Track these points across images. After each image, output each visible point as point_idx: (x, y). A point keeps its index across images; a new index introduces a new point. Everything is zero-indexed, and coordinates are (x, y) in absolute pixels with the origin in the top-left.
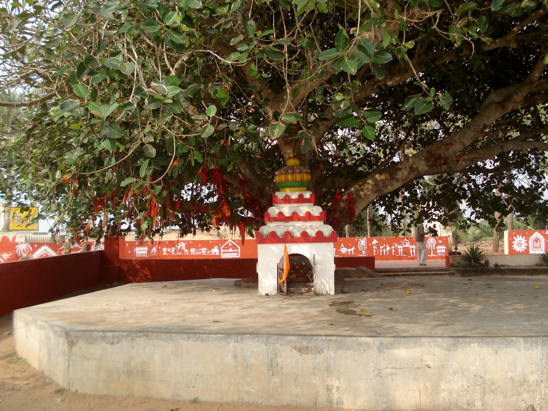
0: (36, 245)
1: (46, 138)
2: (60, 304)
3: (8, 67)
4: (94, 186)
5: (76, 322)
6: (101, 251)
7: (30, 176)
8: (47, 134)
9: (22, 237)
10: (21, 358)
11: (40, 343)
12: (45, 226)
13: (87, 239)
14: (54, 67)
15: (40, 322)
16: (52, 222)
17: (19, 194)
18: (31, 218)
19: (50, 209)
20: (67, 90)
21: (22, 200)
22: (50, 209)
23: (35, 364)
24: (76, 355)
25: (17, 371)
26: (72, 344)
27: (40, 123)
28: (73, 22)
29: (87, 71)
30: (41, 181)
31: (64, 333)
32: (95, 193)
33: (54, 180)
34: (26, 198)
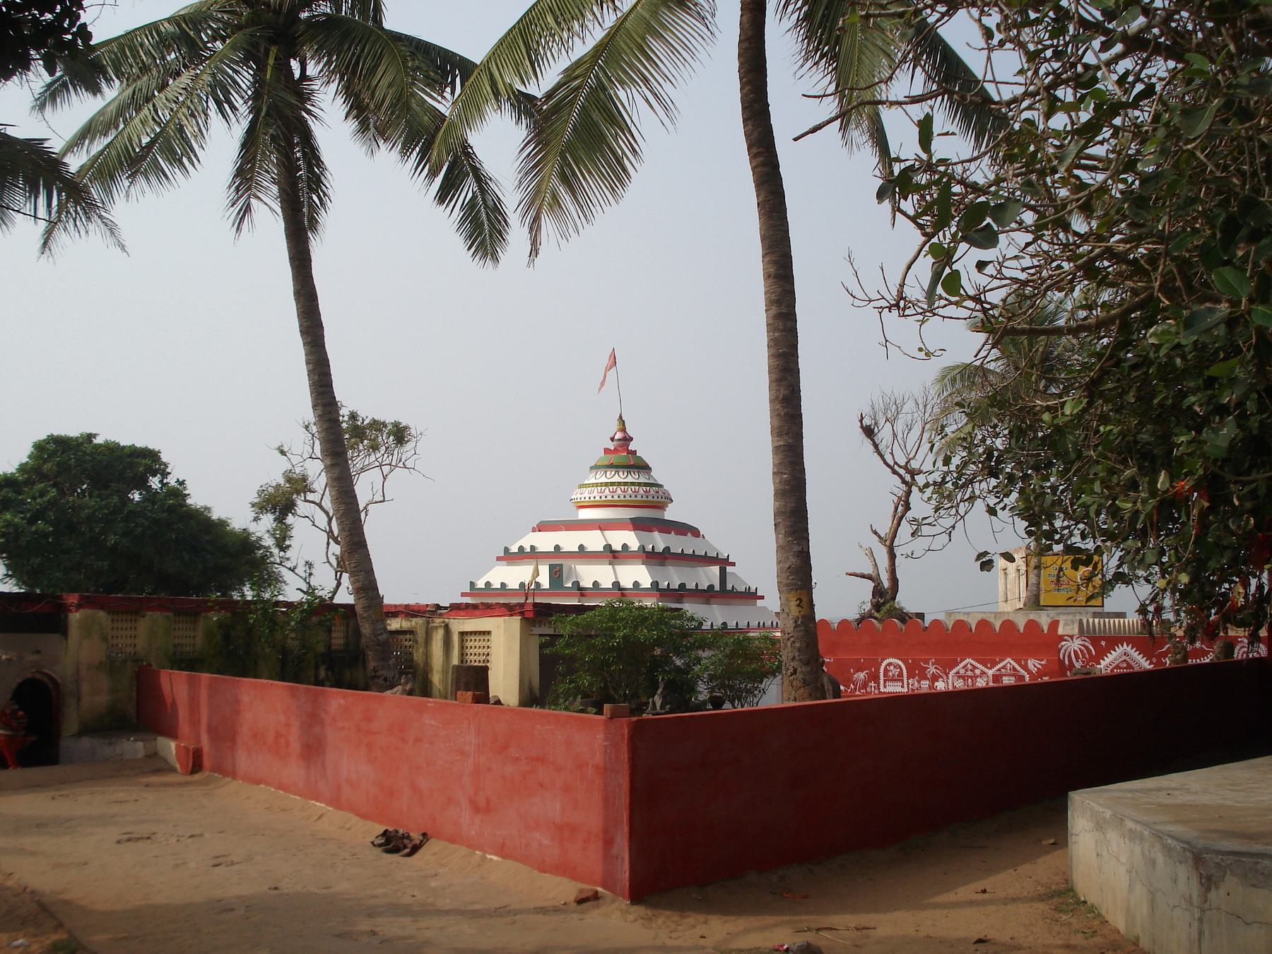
0: (1103, 642)
1: (1131, 398)
2: (1173, 785)
3: (1045, 246)
4: (1248, 505)
5: (1216, 831)
6: (1261, 658)
7: (1097, 487)
8: (1134, 388)
9: (1073, 622)
10: (1085, 902)
11: (1129, 872)
12: (1126, 601)
13: (1226, 630)
14: (1153, 236)
15: (1130, 824)
16: (1144, 591)
17: (1068, 527)
18: (1097, 580)
19: (1142, 560)
20: (1187, 285)
21: (1076, 539)
22: (1142, 560)
23: (1119, 921)
24: (1219, 909)
25: (1077, 931)
26: (1208, 882)
27: (1117, 365)
28: (1203, 127)
29: (1244, 232)
30: (1122, 497)
31: (1188, 854)
32: (1252, 521)
33: (1153, 492)
34: (1083, 537)
